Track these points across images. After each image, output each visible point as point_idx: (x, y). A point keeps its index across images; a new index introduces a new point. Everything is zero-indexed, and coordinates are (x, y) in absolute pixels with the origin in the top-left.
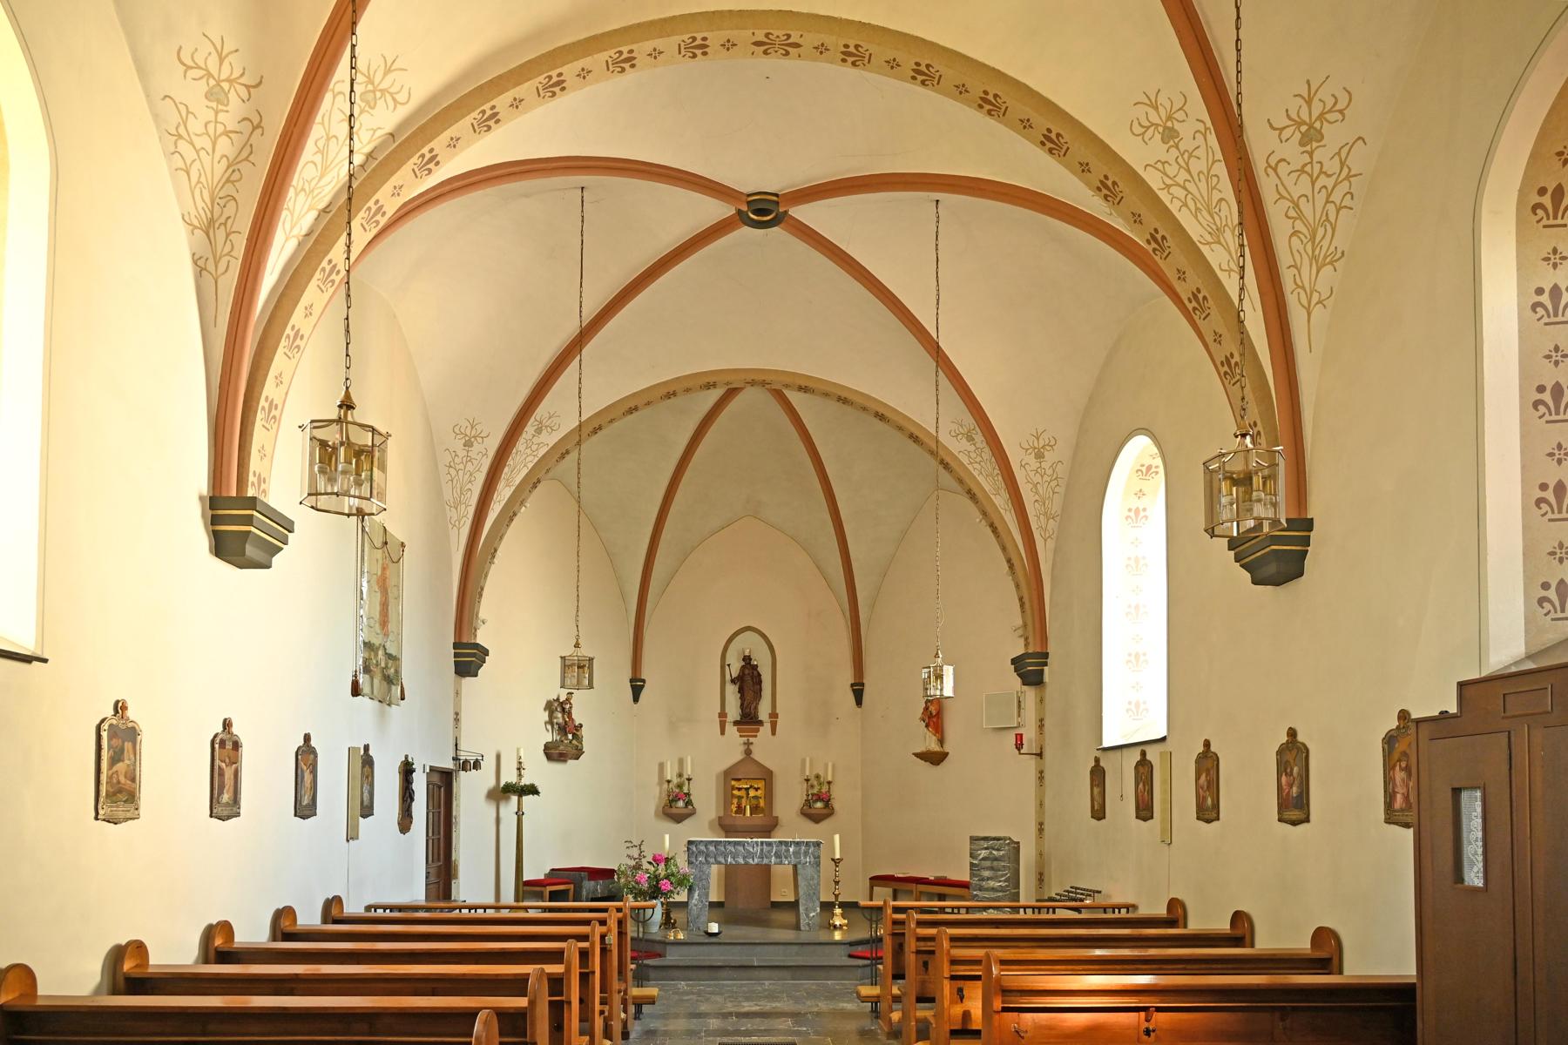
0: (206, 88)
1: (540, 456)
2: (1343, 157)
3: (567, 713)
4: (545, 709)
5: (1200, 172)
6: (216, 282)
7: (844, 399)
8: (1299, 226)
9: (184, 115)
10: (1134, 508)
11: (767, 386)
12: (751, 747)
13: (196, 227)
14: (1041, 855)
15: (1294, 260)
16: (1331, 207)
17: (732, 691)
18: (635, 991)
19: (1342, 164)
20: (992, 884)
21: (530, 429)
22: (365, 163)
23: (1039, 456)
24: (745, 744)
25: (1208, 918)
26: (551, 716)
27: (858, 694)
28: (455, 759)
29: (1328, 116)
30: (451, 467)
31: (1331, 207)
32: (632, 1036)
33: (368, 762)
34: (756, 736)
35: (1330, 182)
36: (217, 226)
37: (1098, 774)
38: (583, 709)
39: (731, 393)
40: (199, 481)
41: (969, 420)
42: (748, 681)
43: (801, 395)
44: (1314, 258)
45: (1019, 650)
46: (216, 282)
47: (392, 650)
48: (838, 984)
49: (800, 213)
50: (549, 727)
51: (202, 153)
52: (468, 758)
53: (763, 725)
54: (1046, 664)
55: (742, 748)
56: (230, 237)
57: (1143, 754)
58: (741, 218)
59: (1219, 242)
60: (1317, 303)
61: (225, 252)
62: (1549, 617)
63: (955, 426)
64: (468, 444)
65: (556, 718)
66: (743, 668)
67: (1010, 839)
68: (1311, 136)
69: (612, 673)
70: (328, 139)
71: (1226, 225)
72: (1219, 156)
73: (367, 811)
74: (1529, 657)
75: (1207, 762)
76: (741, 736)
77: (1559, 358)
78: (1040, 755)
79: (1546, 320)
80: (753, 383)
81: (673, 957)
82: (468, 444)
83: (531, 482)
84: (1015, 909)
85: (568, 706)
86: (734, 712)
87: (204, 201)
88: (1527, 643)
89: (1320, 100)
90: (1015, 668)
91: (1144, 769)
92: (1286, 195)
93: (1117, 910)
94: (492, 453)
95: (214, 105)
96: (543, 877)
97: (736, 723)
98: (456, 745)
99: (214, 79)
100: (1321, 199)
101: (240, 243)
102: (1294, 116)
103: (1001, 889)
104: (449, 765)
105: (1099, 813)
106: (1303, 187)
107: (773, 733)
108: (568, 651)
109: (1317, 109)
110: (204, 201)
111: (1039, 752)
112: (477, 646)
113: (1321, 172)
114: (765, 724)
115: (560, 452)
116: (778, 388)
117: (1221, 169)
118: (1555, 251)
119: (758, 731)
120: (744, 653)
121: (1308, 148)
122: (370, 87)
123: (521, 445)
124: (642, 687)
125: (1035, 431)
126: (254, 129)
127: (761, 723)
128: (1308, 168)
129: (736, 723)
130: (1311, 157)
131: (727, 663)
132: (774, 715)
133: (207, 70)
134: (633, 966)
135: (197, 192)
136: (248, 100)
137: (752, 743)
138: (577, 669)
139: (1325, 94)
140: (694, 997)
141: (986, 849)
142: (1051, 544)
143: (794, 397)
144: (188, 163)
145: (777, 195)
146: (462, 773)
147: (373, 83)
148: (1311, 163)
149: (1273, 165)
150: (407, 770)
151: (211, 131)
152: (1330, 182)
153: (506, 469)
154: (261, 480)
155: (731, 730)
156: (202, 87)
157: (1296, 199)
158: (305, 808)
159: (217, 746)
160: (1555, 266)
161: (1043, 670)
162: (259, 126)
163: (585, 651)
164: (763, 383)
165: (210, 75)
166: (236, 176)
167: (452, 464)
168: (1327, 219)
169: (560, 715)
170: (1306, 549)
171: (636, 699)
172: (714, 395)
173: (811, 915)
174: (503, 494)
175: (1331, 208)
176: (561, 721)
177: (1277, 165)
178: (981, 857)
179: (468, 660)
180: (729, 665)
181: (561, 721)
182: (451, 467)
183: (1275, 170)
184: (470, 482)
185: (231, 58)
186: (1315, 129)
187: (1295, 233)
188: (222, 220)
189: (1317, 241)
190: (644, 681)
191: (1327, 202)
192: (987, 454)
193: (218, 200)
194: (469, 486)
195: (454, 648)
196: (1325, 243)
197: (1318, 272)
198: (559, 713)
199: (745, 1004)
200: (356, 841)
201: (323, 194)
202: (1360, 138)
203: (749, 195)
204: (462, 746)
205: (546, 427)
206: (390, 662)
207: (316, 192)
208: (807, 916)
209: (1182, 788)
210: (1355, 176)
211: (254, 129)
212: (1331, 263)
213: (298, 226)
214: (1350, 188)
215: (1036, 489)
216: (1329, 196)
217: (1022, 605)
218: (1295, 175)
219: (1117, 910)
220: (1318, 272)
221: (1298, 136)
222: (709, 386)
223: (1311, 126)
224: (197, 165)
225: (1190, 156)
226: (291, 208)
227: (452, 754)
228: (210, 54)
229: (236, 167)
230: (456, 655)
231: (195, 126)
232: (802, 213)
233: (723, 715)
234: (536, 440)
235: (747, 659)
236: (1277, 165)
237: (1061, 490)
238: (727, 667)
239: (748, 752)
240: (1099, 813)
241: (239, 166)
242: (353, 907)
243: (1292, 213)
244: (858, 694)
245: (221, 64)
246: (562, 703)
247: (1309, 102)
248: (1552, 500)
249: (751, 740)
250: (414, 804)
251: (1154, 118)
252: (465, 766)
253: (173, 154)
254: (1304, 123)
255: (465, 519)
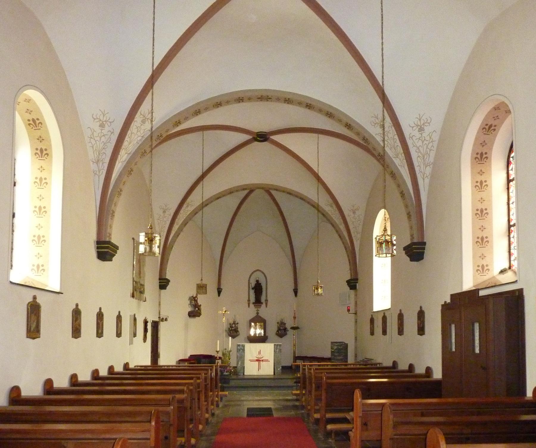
0: (99, 124)
1: (188, 214)
2: (430, 135)
3: (196, 301)
4: (189, 300)
5: (391, 137)
6: (99, 177)
7: (290, 193)
8: (420, 154)
9: (93, 132)
10: (480, 152)
11: (264, 189)
12: (258, 311)
13: (94, 162)
14: (356, 347)
15: (419, 164)
16: (428, 149)
17: (252, 292)
18: (220, 393)
19: (430, 138)
20: (338, 358)
21: (185, 206)
22: (141, 139)
23: (354, 213)
24: (256, 310)
25: (403, 366)
26: (191, 302)
27: (296, 292)
28: (159, 318)
29: (426, 124)
30: (91, 138)
31: (428, 149)
32: (220, 406)
33: (135, 319)
34: (260, 308)
35: (427, 143)
36: (100, 161)
37: (372, 321)
38: (201, 300)
39: (251, 191)
40: (93, 237)
41: (331, 201)
42: (258, 289)
43: (275, 191)
44: (424, 164)
45: (348, 278)
46: (99, 177)
47: (142, 283)
48: (286, 392)
49: (274, 138)
50: (190, 306)
51: (97, 142)
52: (164, 317)
53: (262, 304)
54: (357, 283)
55: (256, 312)
56: (104, 164)
57: (384, 314)
58: (255, 139)
59: (398, 157)
60: (426, 177)
61: (102, 168)
62: (479, 275)
63: (373, 119)
64: (164, 212)
65: (192, 303)
66: (256, 284)
67: (344, 343)
68: (421, 130)
69: (212, 289)
70: (132, 134)
71: (399, 153)
72: (396, 133)
73: (135, 335)
74: (474, 286)
75: (401, 317)
76: (255, 308)
77: (482, 201)
78: (356, 314)
79: (479, 190)
80: (259, 188)
81: (232, 383)
82: (164, 212)
83: (185, 223)
84: (346, 365)
85: (196, 299)
86: (253, 299)
87: (97, 155)
88: (473, 284)
89: (423, 120)
90: (405, 252)
91: (384, 319)
92: (415, 145)
93: (376, 365)
94: (172, 214)
95: (101, 128)
96: (187, 358)
97: (253, 303)
98: (159, 313)
99: (102, 121)
100: (425, 147)
101: (106, 165)
102: (416, 123)
103: (341, 360)
104: (157, 319)
105: (372, 333)
106: (420, 143)
107: (266, 306)
108: (199, 282)
109: (422, 122)
110: (97, 155)
111: (355, 313)
112: (167, 279)
113: (425, 140)
114: (263, 304)
115: (195, 213)
116: (268, 190)
117: (396, 137)
118: (481, 171)
119: (261, 306)
120: (256, 279)
121: (420, 133)
122: (144, 118)
123: (182, 211)
124: (221, 291)
125: (419, 116)
126: (111, 133)
127: (262, 303)
128: (421, 138)
129: (253, 303)
130: (422, 135)
131: (250, 282)
132: (266, 300)
133: (100, 119)
134: (220, 384)
135: (95, 152)
136: (111, 125)
137: (259, 310)
138: (202, 288)
139: (424, 118)
140: (239, 396)
141: (336, 346)
142: (359, 242)
143: (273, 192)
144: (93, 144)
145: (266, 132)
146: (161, 323)
147: (145, 117)
148: (422, 137)
149: (411, 137)
150: (146, 322)
151: (100, 136)
152: (427, 143)
153: (177, 219)
154: (110, 235)
155: (252, 306)
156: (98, 124)
157: (418, 147)
158: (119, 335)
159: (98, 316)
160: (481, 175)
161: (356, 285)
162: (113, 133)
163: (204, 282)
164: (263, 188)
165: (100, 120)
166: (106, 147)
167: (92, 136)
168: (427, 153)
169: (193, 302)
170: (423, 251)
171: (219, 296)
172: (246, 192)
173: (279, 369)
174: (176, 227)
175: (428, 150)
176: (194, 304)
177: (412, 137)
178: (335, 348)
179: (163, 284)
180: (251, 283)
181: (194, 304)
182: (91, 138)
183: (412, 138)
184: (104, 148)
185: (107, 115)
186: (422, 127)
187: (419, 156)
188: (101, 160)
189: (425, 159)
190: (222, 289)
191: (427, 148)
192: (337, 212)
193: (101, 154)
194: (164, 225)
195: (159, 280)
196: (427, 160)
197: (426, 168)
198: (194, 301)
199: (255, 397)
200: (132, 345)
201: (130, 149)
202: (434, 131)
203: (257, 133)
204: (161, 314)
205: (147, 119)
206: (142, 286)
207: (127, 149)
208: (277, 370)
209: (411, 324)
210: (434, 141)
211: (111, 133)
212: (429, 165)
213: (122, 159)
214: (433, 145)
215: (354, 223)
216: (427, 147)
217: (350, 262)
218: (418, 140)
219: (376, 365)
220: (426, 168)
221: (417, 129)
222: (244, 189)
223: (421, 127)
224: (95, 145)
225: (388, 132)
226: (120, 154)
227: (158, 316)
228: (101, 115)
229: (106, 144)
230: (160, 282)
231: (95, 134)
232: (274, 138)
233: (249, 300)
234: (186, 209)
235: (257, 281)
236: (412, 137)
237: (361, 224)
238: (250, 284)
239: (258, 313)
240: (372, 333)
241: (107, 144)
242: (131, 366)
243: (417, 151)
244: (296, 292)
245: (104, 117)
246: (194, 297)
247: (420, 120)
248: (480, 241)
249: (259, 309)
250: (147, 333)
251: (377, 121)
252: (162, 320)
253: (89, 143)
254: (419, 126)
255: (163, 236)
